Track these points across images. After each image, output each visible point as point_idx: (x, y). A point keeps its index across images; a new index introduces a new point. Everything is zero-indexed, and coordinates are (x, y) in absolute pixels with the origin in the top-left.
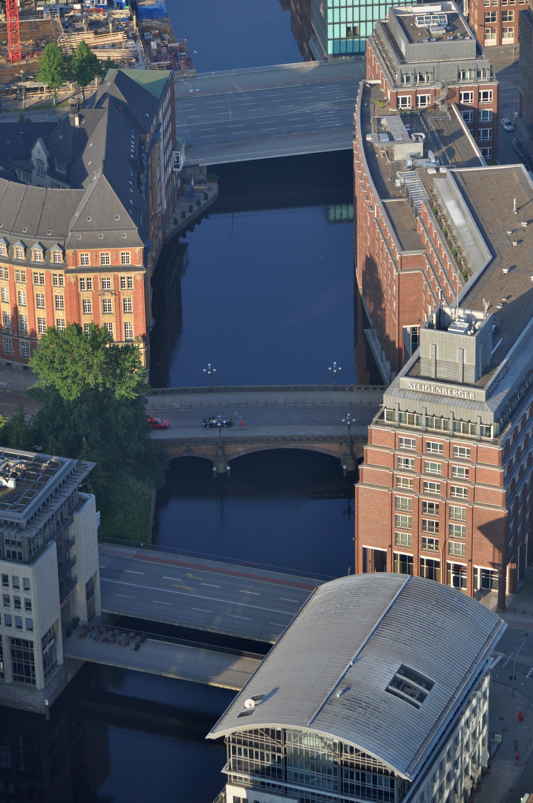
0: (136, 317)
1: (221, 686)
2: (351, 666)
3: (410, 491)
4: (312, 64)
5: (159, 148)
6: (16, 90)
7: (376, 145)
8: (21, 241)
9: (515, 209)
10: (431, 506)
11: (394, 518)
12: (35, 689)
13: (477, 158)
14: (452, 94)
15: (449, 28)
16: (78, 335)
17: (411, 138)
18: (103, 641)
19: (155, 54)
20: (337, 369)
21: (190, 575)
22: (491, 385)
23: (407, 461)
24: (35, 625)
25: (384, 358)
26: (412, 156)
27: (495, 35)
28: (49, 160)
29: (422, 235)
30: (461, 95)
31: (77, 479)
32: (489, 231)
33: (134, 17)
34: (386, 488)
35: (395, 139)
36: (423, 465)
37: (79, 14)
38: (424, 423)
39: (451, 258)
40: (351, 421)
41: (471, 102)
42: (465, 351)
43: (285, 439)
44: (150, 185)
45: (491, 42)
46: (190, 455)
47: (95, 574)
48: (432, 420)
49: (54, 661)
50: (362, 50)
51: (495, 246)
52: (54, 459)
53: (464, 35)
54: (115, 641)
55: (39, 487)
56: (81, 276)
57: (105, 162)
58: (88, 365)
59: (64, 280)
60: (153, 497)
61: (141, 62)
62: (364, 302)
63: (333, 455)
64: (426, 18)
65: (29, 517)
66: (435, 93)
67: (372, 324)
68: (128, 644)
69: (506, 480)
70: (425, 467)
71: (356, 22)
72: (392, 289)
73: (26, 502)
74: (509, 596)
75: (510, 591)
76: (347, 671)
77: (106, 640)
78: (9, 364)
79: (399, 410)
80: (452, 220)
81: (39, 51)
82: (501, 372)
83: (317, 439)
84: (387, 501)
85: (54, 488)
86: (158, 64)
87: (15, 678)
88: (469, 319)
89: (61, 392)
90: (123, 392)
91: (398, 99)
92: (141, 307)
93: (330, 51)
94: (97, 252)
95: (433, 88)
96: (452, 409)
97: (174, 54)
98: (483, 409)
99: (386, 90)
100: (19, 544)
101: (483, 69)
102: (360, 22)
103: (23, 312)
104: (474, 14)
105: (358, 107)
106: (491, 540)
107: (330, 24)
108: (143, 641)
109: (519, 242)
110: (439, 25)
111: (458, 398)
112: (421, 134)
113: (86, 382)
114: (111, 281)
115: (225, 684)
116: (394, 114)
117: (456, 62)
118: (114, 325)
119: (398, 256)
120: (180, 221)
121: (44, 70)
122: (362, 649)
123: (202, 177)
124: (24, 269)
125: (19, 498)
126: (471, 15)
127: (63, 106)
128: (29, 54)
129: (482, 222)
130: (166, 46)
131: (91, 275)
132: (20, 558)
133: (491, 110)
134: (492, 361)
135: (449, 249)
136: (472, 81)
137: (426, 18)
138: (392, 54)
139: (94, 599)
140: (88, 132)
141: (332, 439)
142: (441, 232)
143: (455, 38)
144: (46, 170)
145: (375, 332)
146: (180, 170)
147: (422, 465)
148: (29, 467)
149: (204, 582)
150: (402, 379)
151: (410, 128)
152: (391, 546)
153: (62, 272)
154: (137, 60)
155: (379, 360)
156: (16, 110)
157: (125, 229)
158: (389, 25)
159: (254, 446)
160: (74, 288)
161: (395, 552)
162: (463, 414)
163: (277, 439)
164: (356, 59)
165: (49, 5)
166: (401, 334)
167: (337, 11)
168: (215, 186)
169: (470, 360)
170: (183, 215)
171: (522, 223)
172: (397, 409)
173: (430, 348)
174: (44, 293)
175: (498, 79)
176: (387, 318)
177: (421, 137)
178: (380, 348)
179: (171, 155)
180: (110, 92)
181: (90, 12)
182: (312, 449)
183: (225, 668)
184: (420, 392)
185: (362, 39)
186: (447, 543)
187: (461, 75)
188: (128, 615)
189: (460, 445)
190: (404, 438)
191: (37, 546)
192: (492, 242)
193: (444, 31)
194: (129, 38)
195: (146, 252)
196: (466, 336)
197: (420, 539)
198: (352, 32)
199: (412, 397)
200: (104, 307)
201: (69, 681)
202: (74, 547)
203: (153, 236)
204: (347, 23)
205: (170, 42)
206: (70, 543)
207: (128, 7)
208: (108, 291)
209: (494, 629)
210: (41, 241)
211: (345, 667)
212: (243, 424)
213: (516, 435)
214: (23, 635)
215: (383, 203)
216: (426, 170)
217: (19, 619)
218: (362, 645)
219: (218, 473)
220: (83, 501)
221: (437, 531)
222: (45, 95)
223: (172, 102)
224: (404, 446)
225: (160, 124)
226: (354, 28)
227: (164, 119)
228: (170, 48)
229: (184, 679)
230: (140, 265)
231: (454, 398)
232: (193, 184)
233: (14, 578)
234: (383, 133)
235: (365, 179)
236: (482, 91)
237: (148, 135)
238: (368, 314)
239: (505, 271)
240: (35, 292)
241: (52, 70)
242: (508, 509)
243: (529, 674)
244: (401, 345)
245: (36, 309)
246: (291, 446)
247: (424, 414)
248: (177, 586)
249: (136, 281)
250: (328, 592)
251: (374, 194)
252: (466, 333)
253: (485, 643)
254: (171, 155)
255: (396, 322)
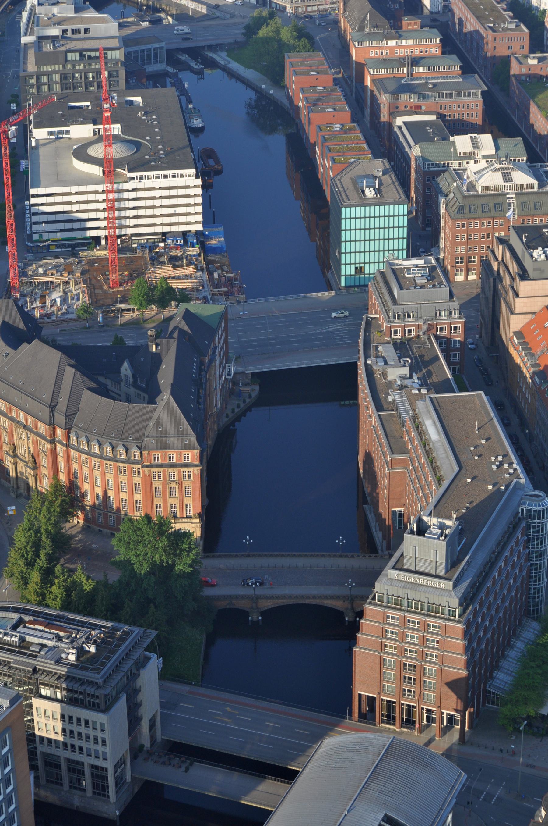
0: (194, 500)
1: (249, 804)
2: (346, 815)
3: (394, 655)
4: (328, 294)
5: (215, 365)
6: (114, 310)
7: (374, 368)
8: (110, 443)
9: (476, 428)
10: (410, 665)
11: (382, 673)
12: (109, 802)
13: (449, 378)
14: (431, 327)
15: (429, 278)
16: (148, 524)
17: (400, 362)
18: (161, 764)
19: (216, 282)
20: (342, 542)
21: (228, 709)
22: (457, 578)
23: (392, 632)
24: (109, 756)
25: (378, 529)
26: (400, 377)
27: (463, 273)
28: (134, 376)
29: (408, 443)
30: (437, 328)
31: (142, 644)
32: (457, 446)
33: (202, 254)
34: (376, 651)
35: (389, 363)
36: (404, 636)
37: (163, 251)
38: (406, 605)
39: (428, 465)
40: (352, 586)
41: (445, 333)
42: (438, 552)
43: (303, 597)
44: (208, 393)
45: (460, 278)
46: (232, 607)
47: (157, 712)
48: (412, 603)
49: (124, 779)
50: (366, 284)
51: (462, 459)
52: (126, 628)
53: (441, 283)
54: (170, 765)
55: (113, 652)
56: (153, 470)
57: (172, 385)
58: (155, 547)
59: (141, 472)
60: (204, 641)
61: (206, 289)
62: (364, 483)
63: (339, 609)
64: (413, 270)
65: (105, 677)
66: (419, 327)
67: (369, 501)
68: (180, 767)
69: (468, 649)
70: (406, 637)
71: (362, 263)
72: (384, 481)
73: (103, 664)
74: (468, 731)
75: (469, 728)
76: (343, 819)
77: (163, 763)
78: (100, 531)
79: (387, 594)
80: (429, 435)
81: (132, 280)
82: (464, 566)
83: (326, 597)
84: (377, 661)
85: (125, 652)
86: (218, 291)
87: (94, 793)
88: (442, 527)
89: (135, 566)
90: (181, 568)
91: (391, 331)
92: (198, 493)
93: (343, 284)
94: (165, 453)
95: (417, 323)
96: (427, 595)
97: (230, 282)
98: (451, 596)
99: (383, 323)
100: (97, 697)
101: (454, 309)
102: (365, 263)
103: (111, 494)
104: (448, 257)
105: (362, 334)
106: (456, 693)
107: (343, 242)
108: (191, 764)
109: (479, 456)
110: (422, 276)
111: (432, 587)
112: (408, 359)
113: (154, 559)
114: (176, 474)
115: (252, 802)
116: (388, 343)
117: (434, 304)
118: (178, 505)
119: (389, 459)
120: (231, 415)
121: (134, 297)
122: (355, 800)
123: (247, 381)
124: (112, 463)
125: (98, 661)
126: (446, 258)
127: (149, 323)
128: (125, 282)
129: (452, 439)
130: (225, 276)
131: (161, 470)
132: (98, 707)
133: (460, 339)
134: (458, 557)
135: (427, 458)
136: (446, 318)
137: (413, 270)
138: (387, 297)
139: (155, 729)
140: (162, 356)
141: (337, 598)
142: (421, 443)
143: (434, 286)
144: (131, 383)
145: (372, 507)
146: (231, 377)
147: (403, 636)
148: (107, 635)
149: (239, 715)
150: (389, 571)
151: (400, 354)
152: (379, 693)
153: (140, 466)
154: (203, 287)
155: (374, 530)
156: (114, 325)
157: (187, 436)
158: (386, 273)
159: (280, 601)
160: (148, 479)
161: (382, 697)
162: (435, 599)
163: (296, 597)
164: (361, 290)
165: (141, 244)
166: (390, 515)
167: (348, 255)
168: (257, 388)
169: (441, 557)
170: (233, 411)
171: (482, 441)
172: (385, 594)
173: (411, 549)
174: (126, 481)
175: (465, 317)
176: (380, 500)
177: (408, 361)
178: (375, 520)
179: (225, 367)
180: (179, 325)
181: (171, 249)
182: (322, 605)
183: (252, 789)
184: (403, 581)
185: (366, 276)
186: (422, 693)
187: (438, 313)
188: (181, 742)
189: (433, 622)
190: (391, 615)
191: (111, 697)
192: (459, 456)
193: (426, 281)
194: (197, 269)
195: (201, 454)
196: (438, 541)
197: (402, 690)
198: (359, 270)
199: (397, 585)
200: (171, 492)
201: (135, 792)
202: (140, 694)
203: (210, 429)
204: (355, 264)
205: (227, 273)
206: (137, 691)
207: (198, 246)
208: (174, 481)
209: (456, 780)
210: (124, 443)
211: (341, 816)
212: (271, 584)
213: (475, 613)
214: (100, 763)
215: (379, 415)
216: (411, 390)
217: (96, 752)
218: (355, 797)
219: (252, 621)
220: (148, 659)
221: (414, 684)
222: (136, 314)
223: (226, 329)
224: (390, 621)
225: (216, 347)
226: (361, 268)
227: (219, 342)
228: (228, 277)
229: (221, 797)
230: (198, 463)
231: (428, 586)
232: (241, 385)
233: (93, 722)
234: (379, 358)
235: (366, 394)
236: (453, 326)
237: (207, 358)
238: (366, 493)
239: (469, 480)
240: (120, 480)
241: (140, 298)
242: (469, 671)
243: (482, 797)
244: (390, 523)
245: (120, 492)
246: (307, 602)
247: (406, 598)
248: (219, 718)
249: (194, 474)
250: (330, 747)
251: (372, 407)
252: (438, 539)
253: (449, 793)
254: (225, 367)
255: (387, 505)
